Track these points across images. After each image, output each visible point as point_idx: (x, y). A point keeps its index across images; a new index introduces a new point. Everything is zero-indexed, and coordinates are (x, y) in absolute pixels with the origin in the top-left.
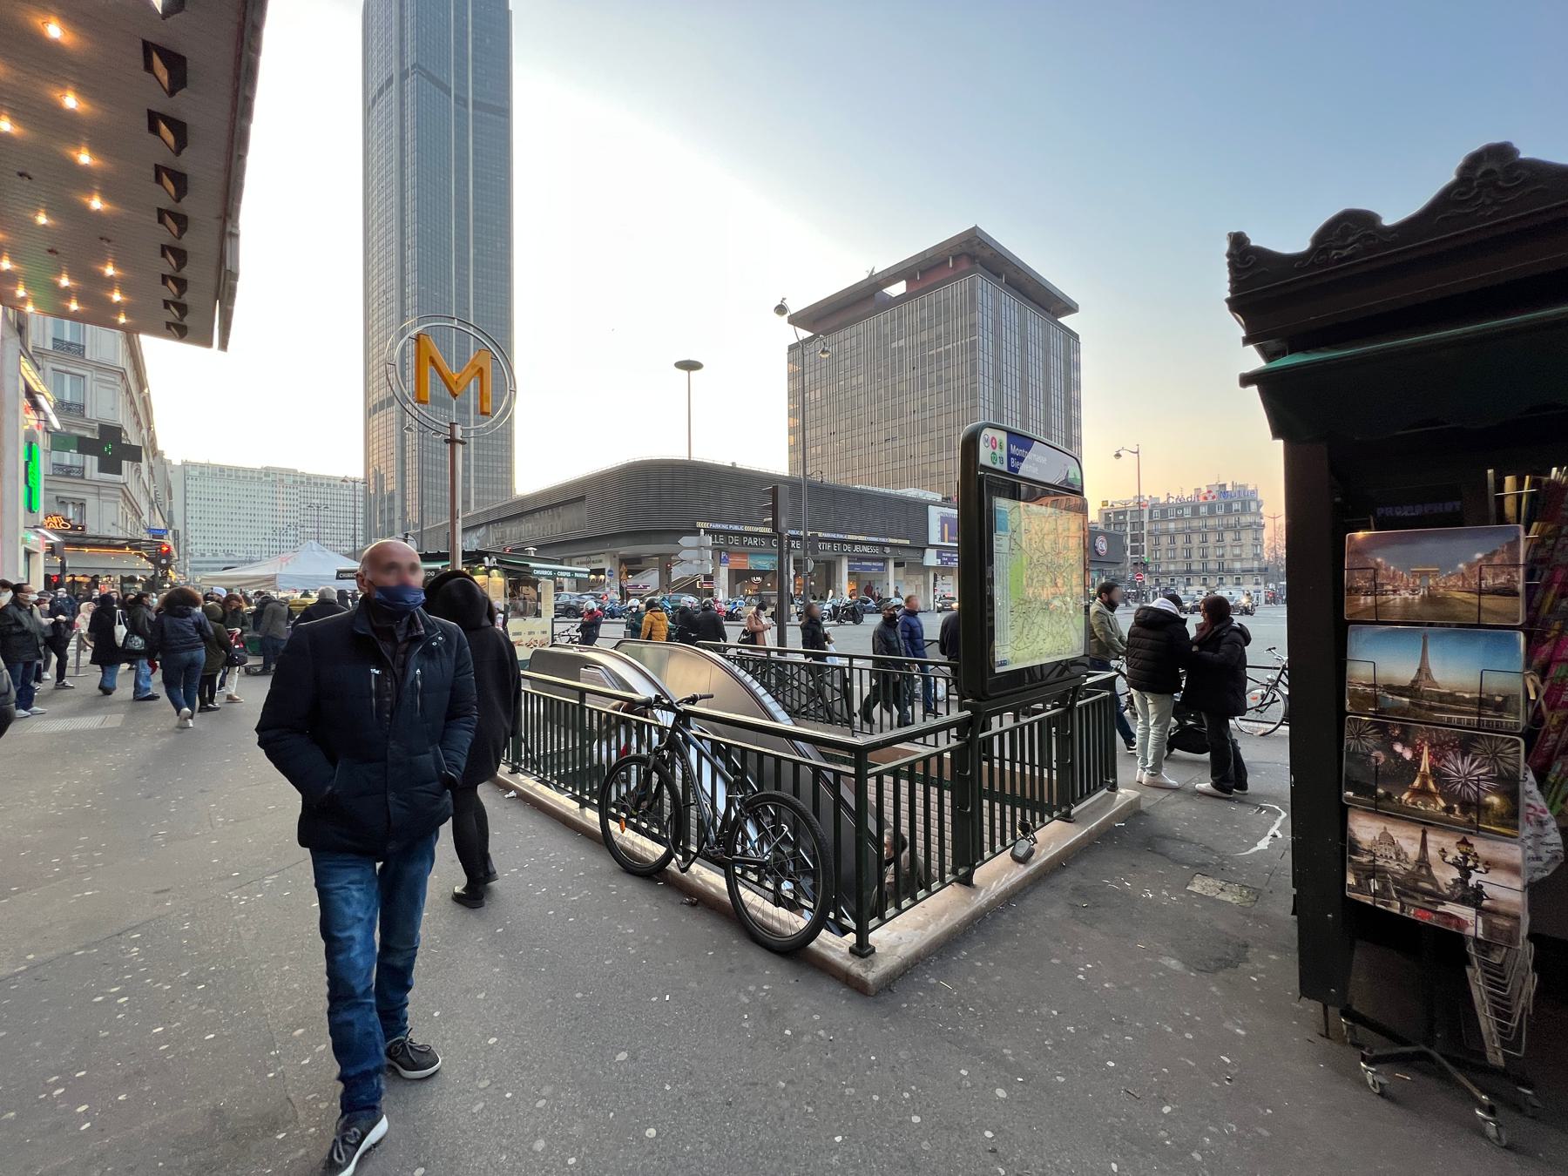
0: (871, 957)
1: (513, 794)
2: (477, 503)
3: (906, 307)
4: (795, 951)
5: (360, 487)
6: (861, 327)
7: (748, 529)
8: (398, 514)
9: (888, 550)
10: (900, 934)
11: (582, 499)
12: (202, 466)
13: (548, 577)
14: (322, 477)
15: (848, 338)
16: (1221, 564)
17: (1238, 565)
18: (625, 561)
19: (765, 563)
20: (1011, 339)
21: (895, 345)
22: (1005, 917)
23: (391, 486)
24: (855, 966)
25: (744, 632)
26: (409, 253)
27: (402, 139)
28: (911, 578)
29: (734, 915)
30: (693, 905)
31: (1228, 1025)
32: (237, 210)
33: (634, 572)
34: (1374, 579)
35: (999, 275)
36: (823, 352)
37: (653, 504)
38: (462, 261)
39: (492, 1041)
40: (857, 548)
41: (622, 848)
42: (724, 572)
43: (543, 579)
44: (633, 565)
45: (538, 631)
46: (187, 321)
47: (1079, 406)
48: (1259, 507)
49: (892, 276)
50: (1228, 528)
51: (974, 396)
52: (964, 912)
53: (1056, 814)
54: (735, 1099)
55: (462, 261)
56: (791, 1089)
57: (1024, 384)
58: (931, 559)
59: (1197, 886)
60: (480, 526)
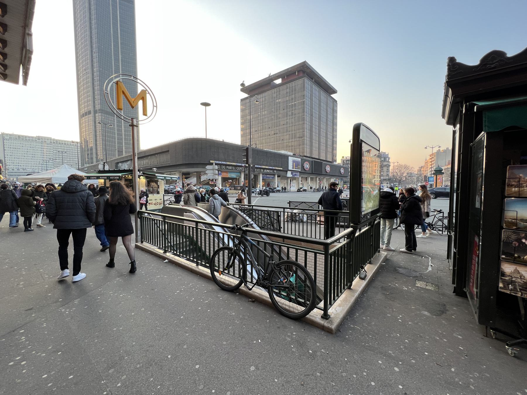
0: (330, 319)
1: (166, 261)
3: (281, 88)
4: (300, 319)
5: (79, 145)
6: (266, 94)
7: (228, 163)
8: (94, 156)
9: (275, 171)
10: (338, 309)
11: (168, 151)
12: (10, 135)
13: (162, 179)
14: (62, 141)
15: (261, 97)
18: (184, 174)
19: (234, 175)
21: (277, 101)
22: (364, 299)
23: (91, 144)
25: (237, 199)
26: (94, 55)
27: (90, 9)
28: (283, 181)
29: (274, 307)
30: (253, 302)
31: (454, 335)
32: (31, 24)
33: (186, 178)
34: (519, 181)
35: (312, 79)
36: (257, 101)
37: (194, 154)
38: (117, 60)
39: (197, 367)
40: (265, 171)
41: (220, 281)
42: (220, 179)
43: (160, 180)
44: (187, 175)
45: (158, 199)
46: (7, 72)
49: (277, 76)
51: (304, 120)
52: (353, 299)
54: (304, 382)
55: (117, 60)
56: (323, 376)
58: (289, 174)
59: (419, 284)
60: (128, 161)
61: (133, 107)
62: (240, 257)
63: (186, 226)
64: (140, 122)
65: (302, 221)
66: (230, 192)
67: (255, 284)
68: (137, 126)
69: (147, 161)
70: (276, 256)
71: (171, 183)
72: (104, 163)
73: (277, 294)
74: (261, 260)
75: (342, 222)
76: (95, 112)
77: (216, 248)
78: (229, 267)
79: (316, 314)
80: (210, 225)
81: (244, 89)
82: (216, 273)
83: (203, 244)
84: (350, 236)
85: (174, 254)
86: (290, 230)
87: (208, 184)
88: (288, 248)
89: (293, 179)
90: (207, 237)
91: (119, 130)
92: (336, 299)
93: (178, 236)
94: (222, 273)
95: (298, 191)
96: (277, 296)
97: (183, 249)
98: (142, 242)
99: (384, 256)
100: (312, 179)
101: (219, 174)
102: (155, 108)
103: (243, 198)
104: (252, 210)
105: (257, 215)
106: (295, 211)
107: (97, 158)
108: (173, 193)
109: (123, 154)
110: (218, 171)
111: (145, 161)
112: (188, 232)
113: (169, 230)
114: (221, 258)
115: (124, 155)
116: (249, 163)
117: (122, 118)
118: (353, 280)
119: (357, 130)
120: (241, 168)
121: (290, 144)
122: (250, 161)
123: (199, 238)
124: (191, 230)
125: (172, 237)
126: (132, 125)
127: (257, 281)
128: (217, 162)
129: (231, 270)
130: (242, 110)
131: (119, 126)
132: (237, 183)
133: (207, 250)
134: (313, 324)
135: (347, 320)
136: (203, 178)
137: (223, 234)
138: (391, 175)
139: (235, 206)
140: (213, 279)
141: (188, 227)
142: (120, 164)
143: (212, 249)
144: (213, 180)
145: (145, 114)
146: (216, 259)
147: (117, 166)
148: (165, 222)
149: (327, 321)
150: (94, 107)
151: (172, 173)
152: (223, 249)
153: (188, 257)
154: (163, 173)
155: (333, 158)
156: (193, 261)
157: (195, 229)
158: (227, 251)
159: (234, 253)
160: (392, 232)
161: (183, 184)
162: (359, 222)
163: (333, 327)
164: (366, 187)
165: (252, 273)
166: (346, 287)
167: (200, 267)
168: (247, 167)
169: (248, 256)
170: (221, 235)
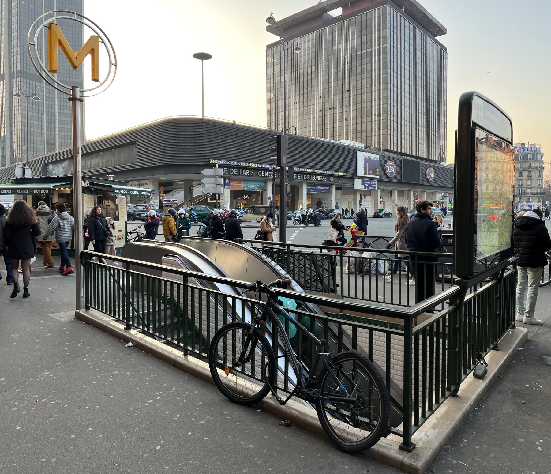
0: (415, 451)
1: (130, 344)
2: (60, 145)
3: (342, 24)
4: (362, 452)
6: (314, 35)
7: (243, 164)
8: (8, 152)
9: (332, 179)
10: (429, 433)
11: (134, 143)
15: (308, 41)
16: (521, 190)
17: (529, 191)
18: (162, 184)
19: (253, 187)
20: (407, 46)
21: (335, 47)
22: (480, 414)
24: (405, 458)
25: (259, 232)
28: (346, 197)
29: (326, 436)
30: (288, 426)
33: (166, 192)
35: (400, 7)
36: (297, 49)
37: (181, 147)
42: (227, 193)
43: (119, 196)
44: (167, 187)
47: (446, 93)
48: (542, 157)
50: (525, 169)
52: (458, 415)
53: (491, 346)
57: (415, 76)
58: (358, 185)
60: (64, 160)
61: (75, 67)
62: (265, 342)
63: (166, 282)
64: (86, 94)
65: (378, 273)
66: (246, 217)
67: (292, 394)
68: (82, 101)
69: (97, 160)
70: (333, 341)
71: (139, 201)
72: (24, 165)
73: (334, 414)
74: (304, 347)
75: (448, 273)
76: (11, 76)
77: (221, 325)
78: (243, 360)
79: (390, 443)
80: (210, 280)
81: (274, 26)
82: (219, 371)
83: (197, 315)
84: (455, 299)
85: (143, 332)
86: (355, 291)
87: (205, 202)
88: (355, 328)
89: (365, 193)
90: (204, 302)
91: (51, 106)
92: (427, 415)
93: (151, 298)
94: (231, 371)
95: (374, 217)
96: (334, 416)
97: (160, 324)
98: (87, 309)
99: (522, 334)
100: (401, 194)
101: (225, 185)
102: (113, 67)
103: (269, 229)
104: (288, 252)
105: (297, 263)
106: (366, 255)
107: (12, 155)
108: (142, 219)
109: (55, 149)
110: (225, 178)
111: (93, 161)
112: (169, 292)
113: (136, 287)
114: (230, 342)
115: (58, 150)
116: (278, 163)
117: (56, 85)
118: (460, 381)
119: (466, 104)
120: (266, 174)
121: (359, 128)
122: (284, 160)
123: (190, 303)
124: (175, 289)
125: (141, 300)
126: (74, 99)
127: (296, 387)
128: (223, 162)
129: (248, 365)
130: (269, 66)
131: (50, 99)
132: (260, 202)
133: (204, 327)
134: (383, 460)
135: (447, 451)
136: (197, 192)
137: (234, 299)
138: (545, 185)
139: (255, 245)
140: (215, 381)
141: (169, 284)
142: (51, 167)
143: (212, 325)
144: (213, 195)
145: (95, 79)
146: (221, 344)
147: (45, 171)
148: (128, 273)
149: (410, 454)
150: (10, 67)
151: (142, 182)
152: (233, 327)
153: (169, 339)
154: (124, 184)
155: (439, 154)
156: (177, 347)
157: (182, 287)
158: (240, 331)
159: (253, 335)
160: (538, 293)
161: (160, 202)
162: (471, 274)
163: (420, 464)
164: (483, 206)
165: (289, 373)
166: (447, 393)
167: (191, 358)
168: (278, 171)
169: (279, 341)
170: (230, 300)
